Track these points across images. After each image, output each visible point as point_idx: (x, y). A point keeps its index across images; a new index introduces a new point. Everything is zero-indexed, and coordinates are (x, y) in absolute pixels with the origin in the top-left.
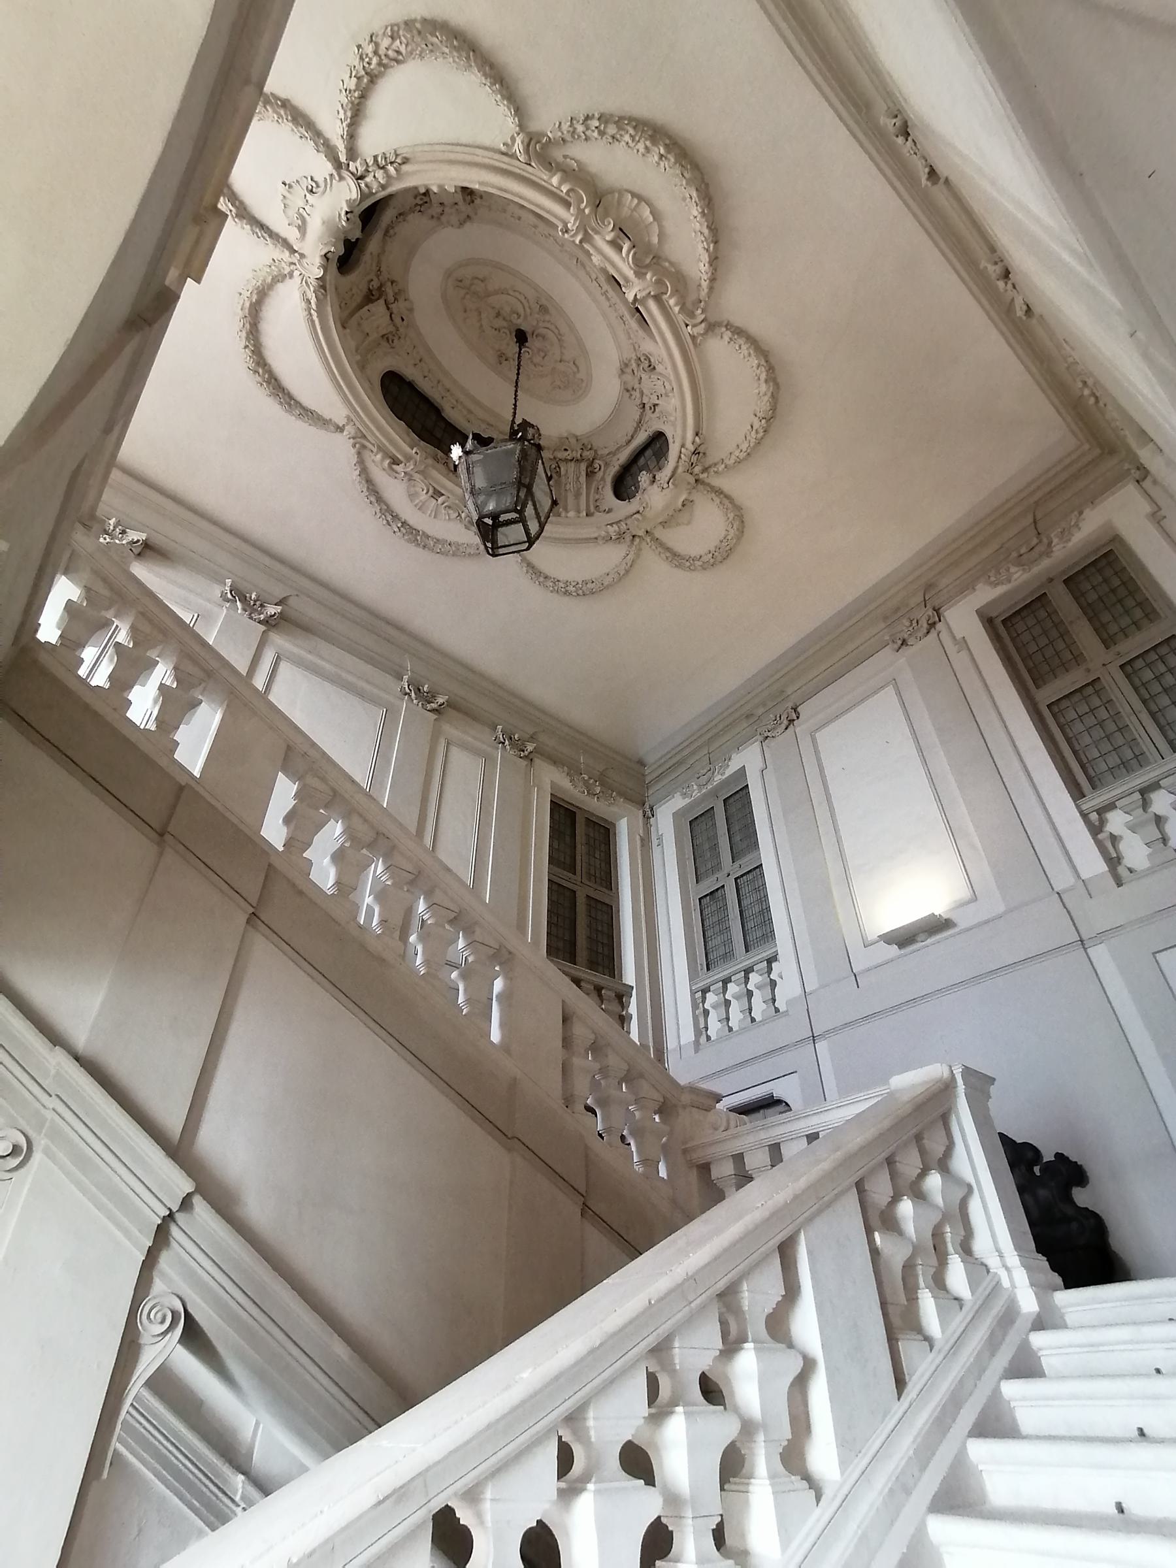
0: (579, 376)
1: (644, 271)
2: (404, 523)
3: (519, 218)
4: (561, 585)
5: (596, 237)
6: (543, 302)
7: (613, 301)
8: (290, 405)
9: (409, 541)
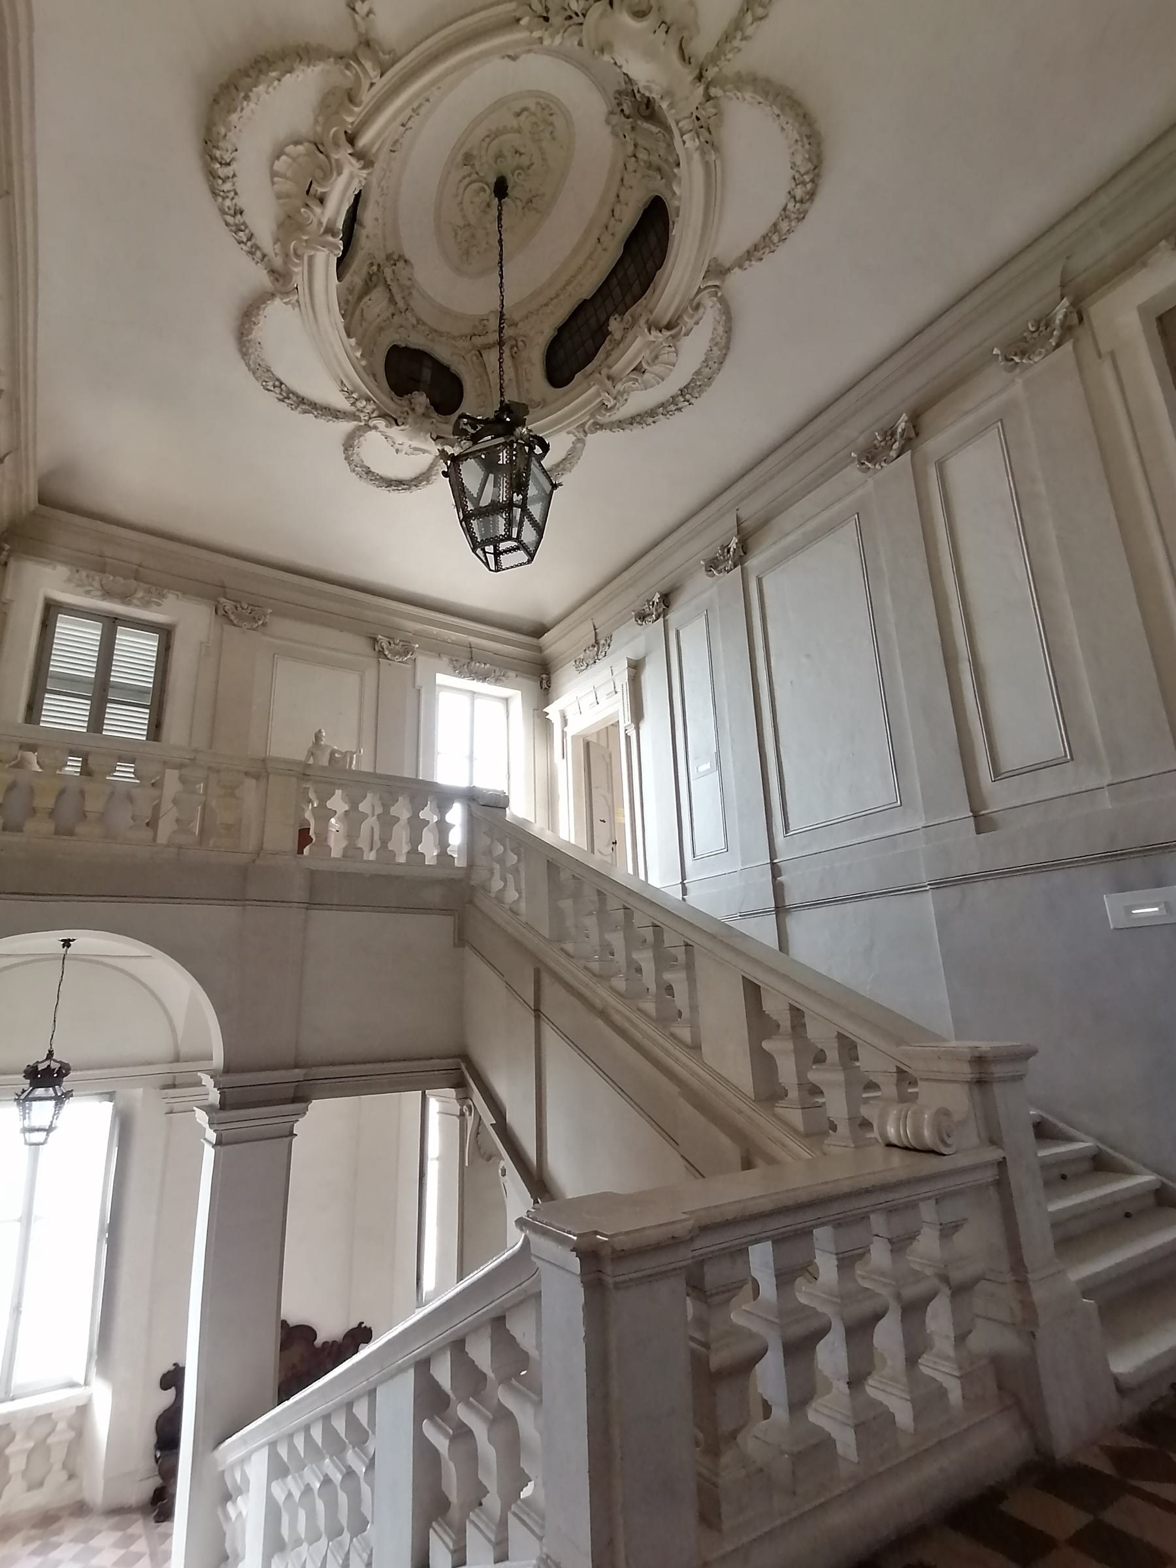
0: (533, 107)
1: (333, 162)
2: (682, 392)
3: (377, 220)
4: (790, 206)
5: (325, 221)
6: (460, 158)
7: (411, 113)
8: (564, 469)
9: (700, 392)
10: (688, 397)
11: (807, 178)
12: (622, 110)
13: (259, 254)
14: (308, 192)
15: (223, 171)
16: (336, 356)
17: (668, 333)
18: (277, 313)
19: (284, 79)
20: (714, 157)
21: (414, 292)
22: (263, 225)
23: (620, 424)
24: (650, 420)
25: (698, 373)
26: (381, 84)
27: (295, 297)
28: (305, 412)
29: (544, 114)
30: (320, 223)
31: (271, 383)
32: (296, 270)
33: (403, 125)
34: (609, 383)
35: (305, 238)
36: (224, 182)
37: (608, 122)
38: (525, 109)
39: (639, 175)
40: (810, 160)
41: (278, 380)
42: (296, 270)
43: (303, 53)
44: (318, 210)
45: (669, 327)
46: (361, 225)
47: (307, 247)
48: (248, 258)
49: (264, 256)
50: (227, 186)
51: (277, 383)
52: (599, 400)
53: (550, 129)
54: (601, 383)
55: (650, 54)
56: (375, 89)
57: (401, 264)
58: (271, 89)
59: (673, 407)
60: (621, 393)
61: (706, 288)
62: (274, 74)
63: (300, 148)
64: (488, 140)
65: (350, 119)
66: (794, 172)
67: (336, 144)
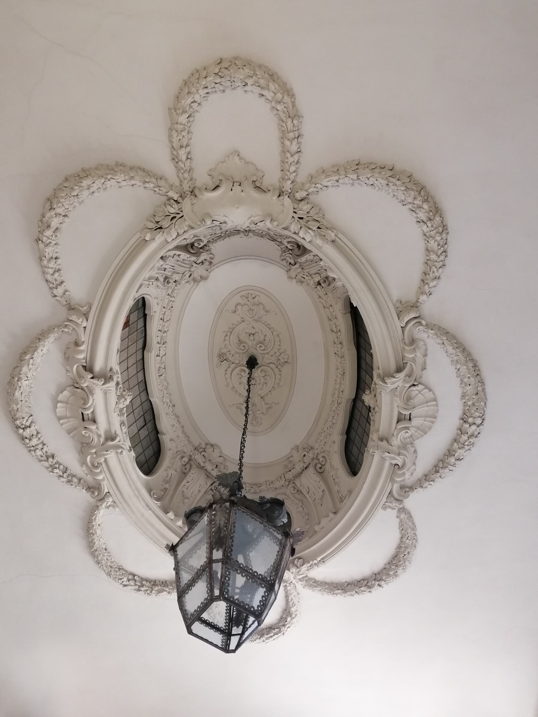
1: (86, 389)
5: (102, 432)
6: (216, 360)
10: (470, 420)
11: (418, 202)
12: (290, 263)
13: (75, 480)
14: (83, 419)
15: (27, 433)
16: (158, 531)
17: (402, 375)
18: (103, 515)
19: (35, 356)
20: (333, 235)
21: (227, 463)
22: (69, 457)
23: (427, 478)
24: (452, 460)
25: (463, 396)
26: (89, 324)
27: (111, 499)
28: (159, 592)
29: (250, 299)
30: (99, 436)
31: (125, 579)
32: (100, 477)
33: (158, 356)
34: (384, 443)
35: (94, 451)
36: (30, 440)
37: (290, 278)
38: (237, 305)
39: (330, 294)
40: (407, 189)
41: (131, 574)
42: (100, 477)
43: (41, 336)
44: (93, 427)
45: (399, 370)
46: (163, 434)
47: (98, 456)
48: (68, 486)
49: (80, 480)
50: (34, 441)
51: (130, 577)
52: (387, 464)
53: (261, 307)
54: (378, 447)
55: (238, 202)
56: (88, 329)
57: (209, 450)
58: (30, 366)
59: (464, 437)
60: (404, 446)
61: (407, 323)
62: (28, 357)
63: (65, 393)
64: (227, 338)
65: (81, 356)
66: (408, 207)
67: (80, 377)
